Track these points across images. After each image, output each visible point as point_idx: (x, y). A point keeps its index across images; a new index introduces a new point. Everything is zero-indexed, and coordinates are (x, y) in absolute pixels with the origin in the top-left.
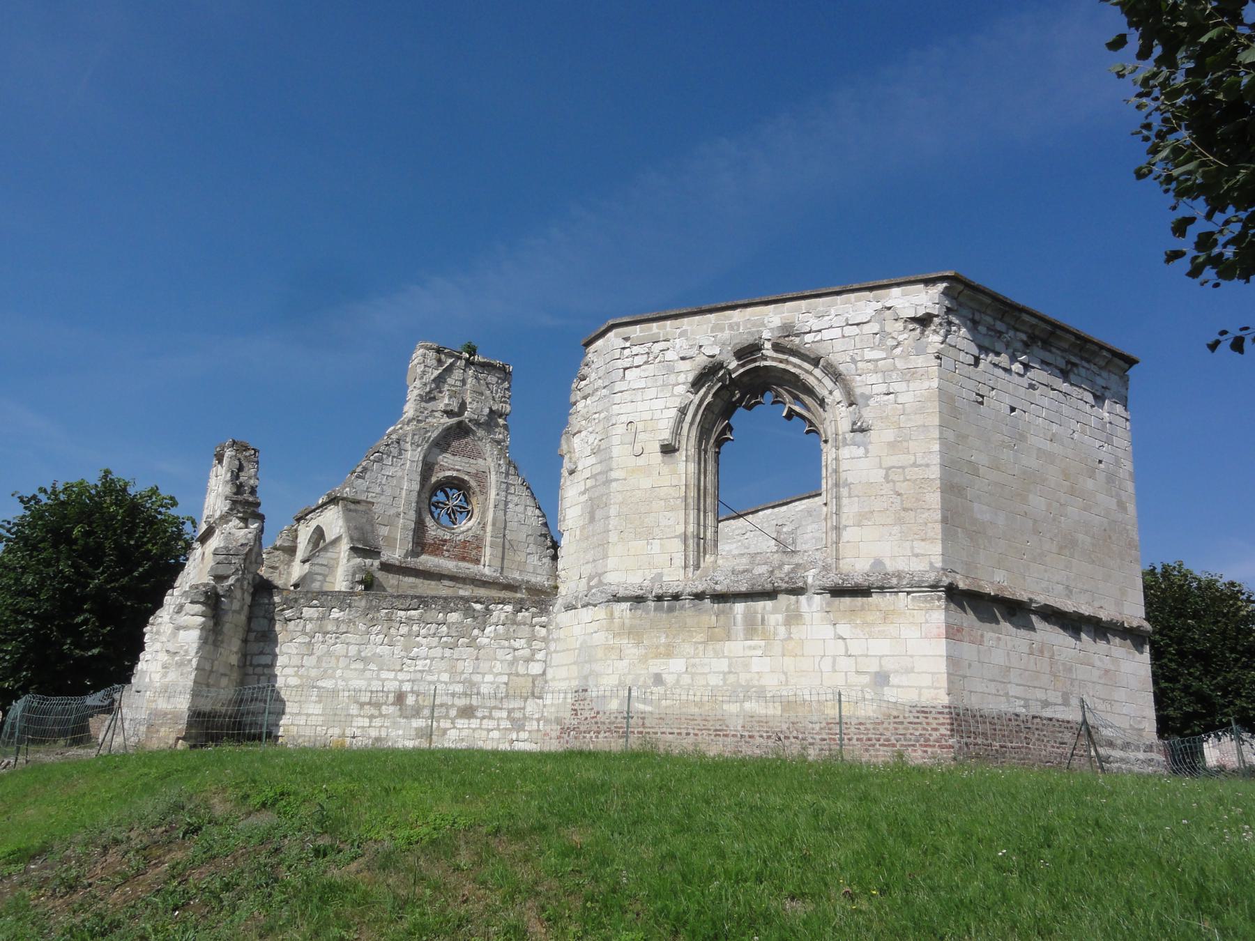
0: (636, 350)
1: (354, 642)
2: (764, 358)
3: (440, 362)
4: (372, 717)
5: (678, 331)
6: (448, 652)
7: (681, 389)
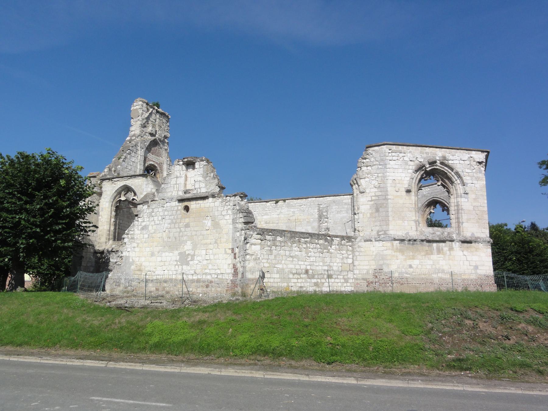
0: (393, 154)
1: (287, 250)
2: (436, 166)
3: (148, 110)
4: (298, 279)
5: (409, 151)
6: (321, 255)
7: (411, 171)
